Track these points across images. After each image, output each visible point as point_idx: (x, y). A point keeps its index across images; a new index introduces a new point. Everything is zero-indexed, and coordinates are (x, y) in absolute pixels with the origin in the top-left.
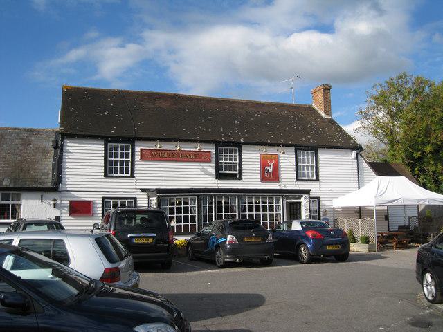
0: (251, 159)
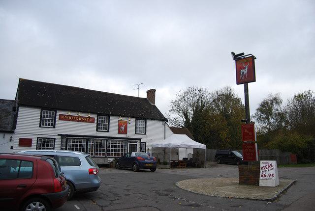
0: (114, 121)
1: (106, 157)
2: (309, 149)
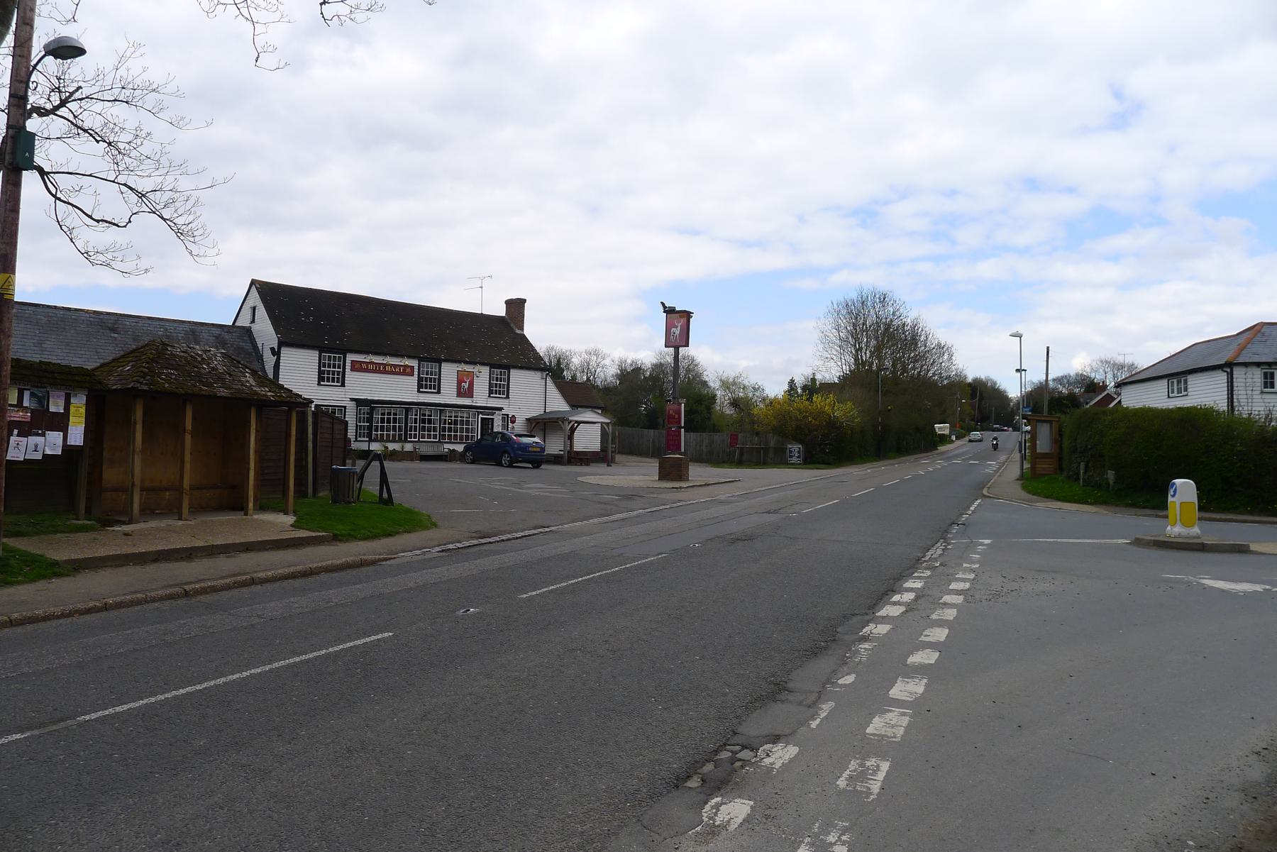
0: (449, 373)
1: (439, 442)
2: (769, 410)
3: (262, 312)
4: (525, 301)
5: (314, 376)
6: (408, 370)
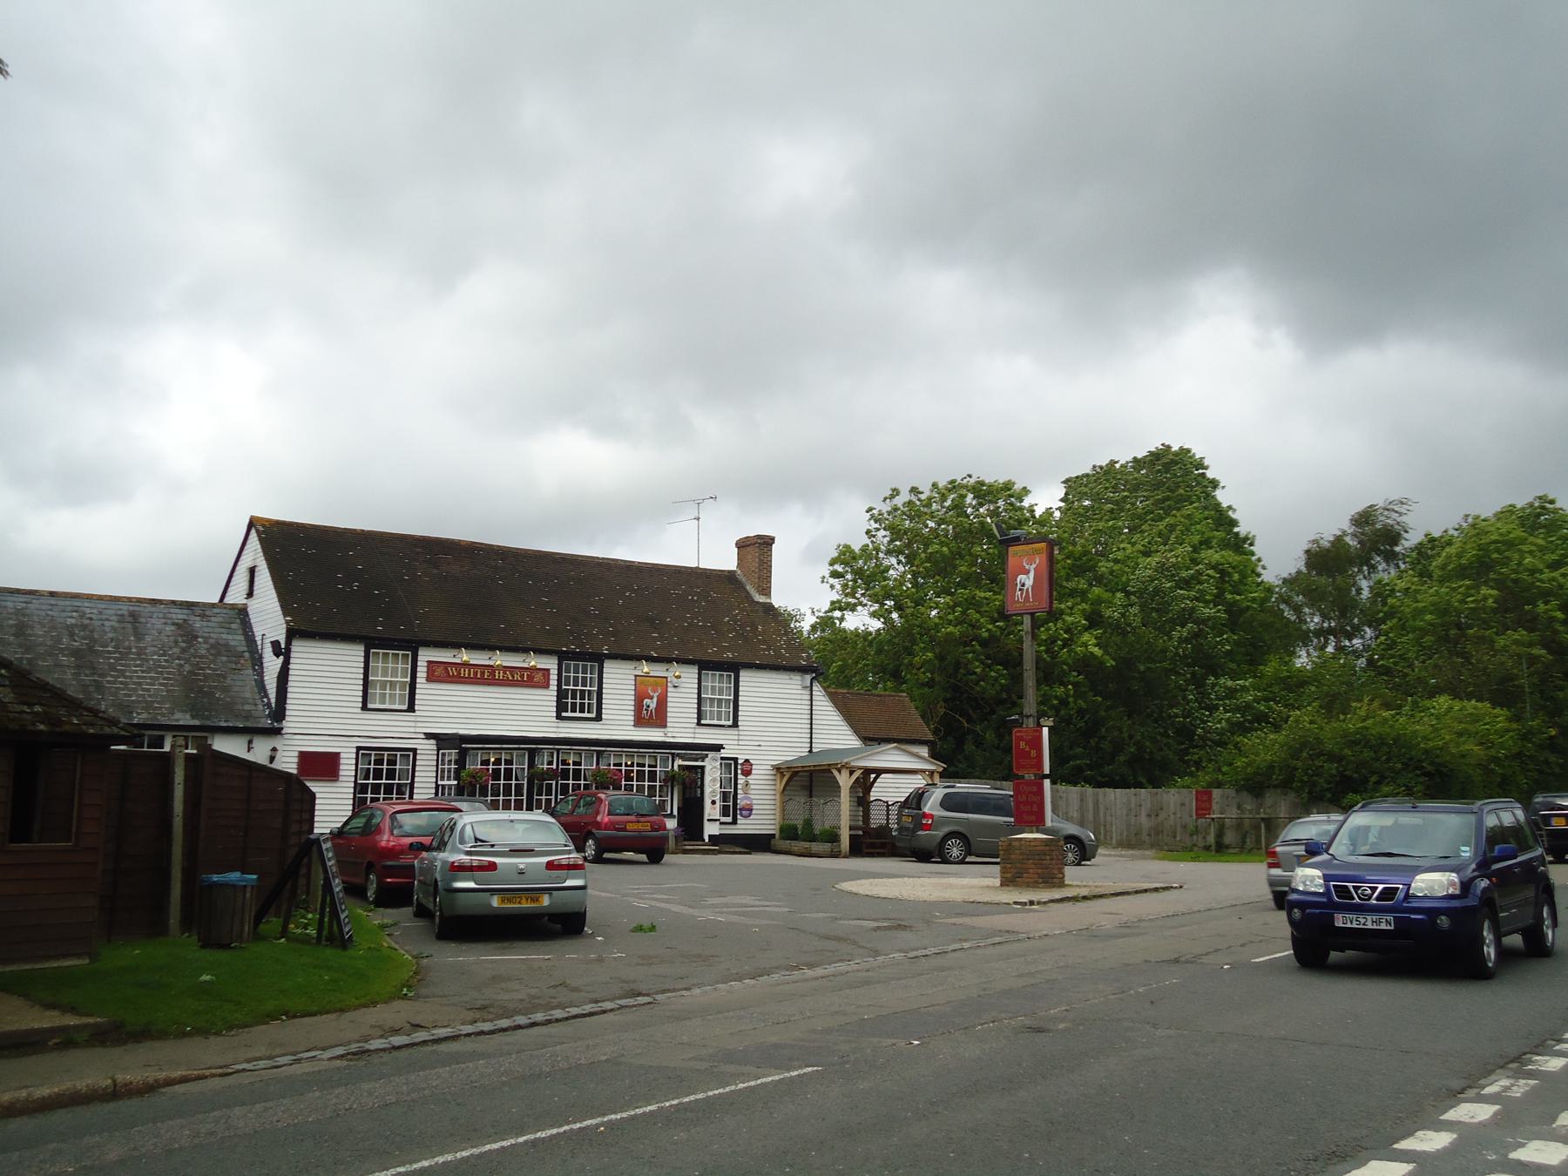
0: (619, 681)
3: (264, 579)
4: (772, 539)
5: (691, 715)
6: (538, 677)
